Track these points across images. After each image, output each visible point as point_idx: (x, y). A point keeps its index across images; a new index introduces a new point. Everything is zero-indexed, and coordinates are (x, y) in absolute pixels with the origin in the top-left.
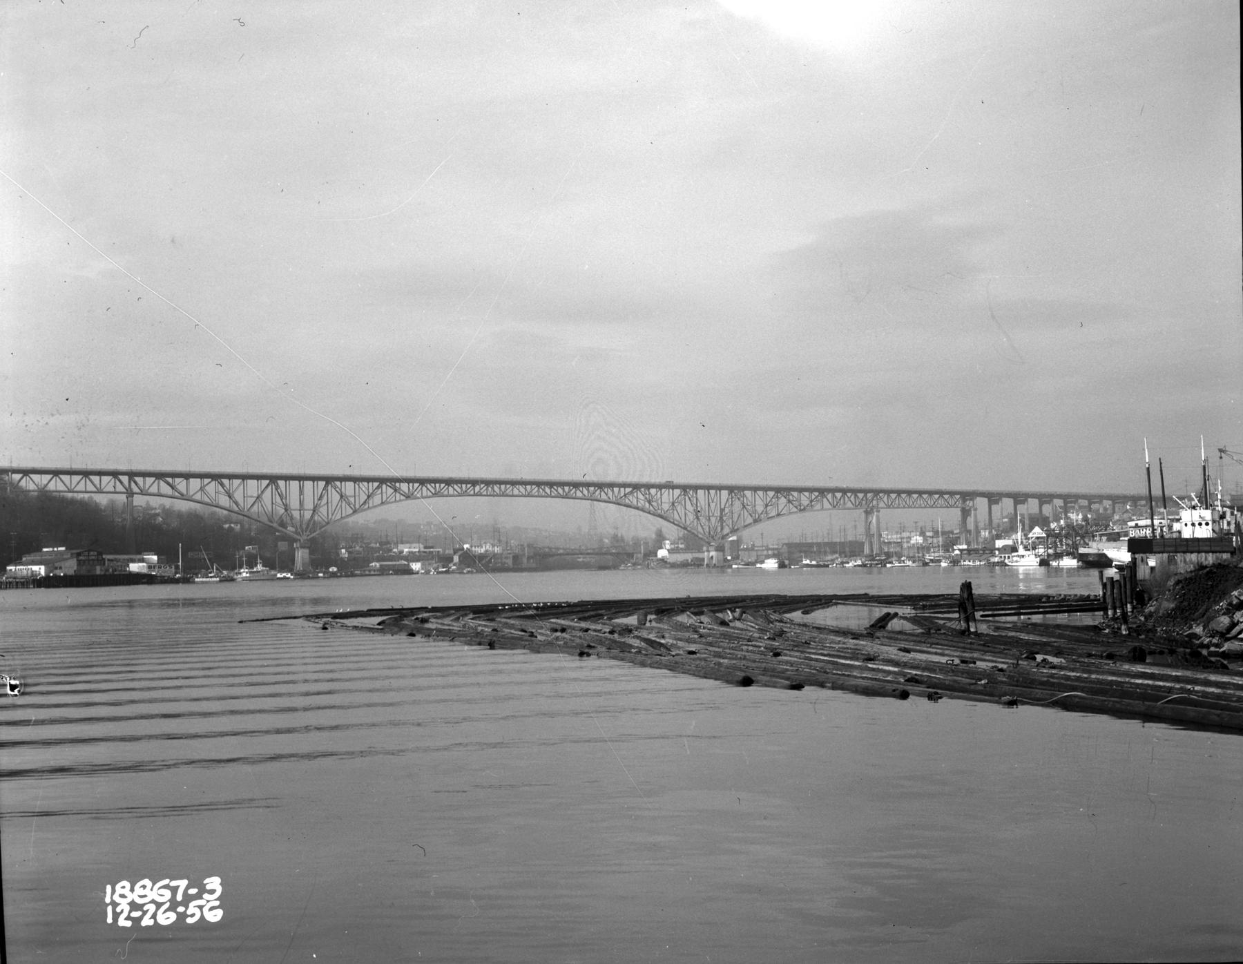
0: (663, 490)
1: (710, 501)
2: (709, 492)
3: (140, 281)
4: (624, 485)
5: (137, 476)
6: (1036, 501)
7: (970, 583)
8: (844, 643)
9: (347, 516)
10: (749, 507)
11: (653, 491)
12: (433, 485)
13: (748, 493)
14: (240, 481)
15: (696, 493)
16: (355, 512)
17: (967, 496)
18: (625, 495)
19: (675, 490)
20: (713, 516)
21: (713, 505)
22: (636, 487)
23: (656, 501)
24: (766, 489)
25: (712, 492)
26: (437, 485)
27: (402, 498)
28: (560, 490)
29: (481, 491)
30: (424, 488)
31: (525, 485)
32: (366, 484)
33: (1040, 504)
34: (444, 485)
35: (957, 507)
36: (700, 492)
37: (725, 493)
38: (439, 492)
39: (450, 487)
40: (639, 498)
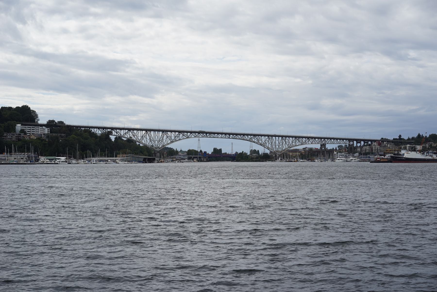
0: (139, 131)
1: (156, 135)
9: (168, 144)
10: (169, 137)
11: (135, 131)
13: (169, 133)
15: (151, 133)
16: (172, 142)
20: (156, 141)
21: (156, 137)
22: (255, 135)
23: (136, 136)
24: (175, 131)
25: (156, 132)
28: (239, 136)
30: (226, 136)
36: (152, 132)
37: (161, 133)
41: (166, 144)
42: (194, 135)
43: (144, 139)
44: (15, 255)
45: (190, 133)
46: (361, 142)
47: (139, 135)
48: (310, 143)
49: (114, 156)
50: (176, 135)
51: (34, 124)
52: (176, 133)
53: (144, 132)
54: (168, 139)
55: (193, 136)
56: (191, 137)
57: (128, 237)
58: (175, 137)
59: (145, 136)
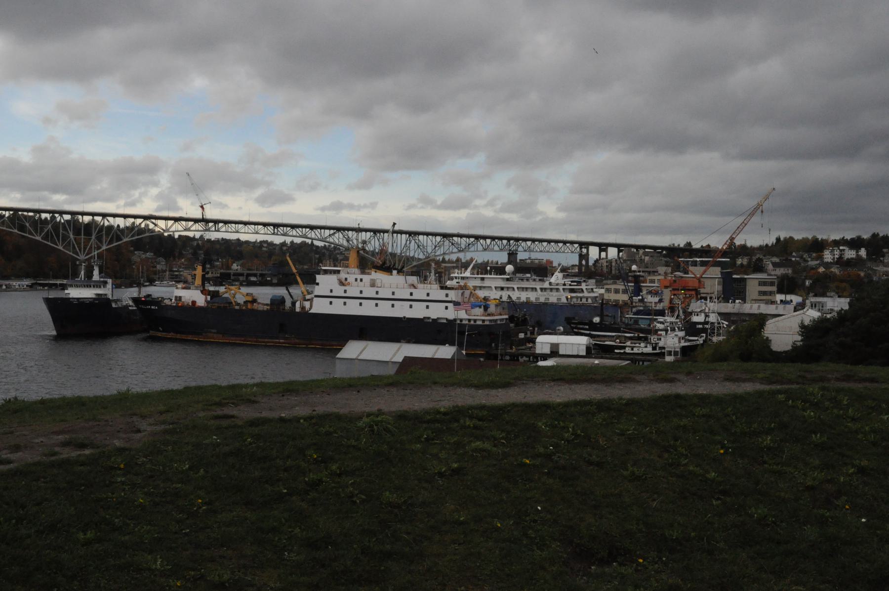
3: (620, 343)
4: (330, 228)
5: (64, 214)
6: (597, 249)
11: (421, 237)
13: (455, 238)
14: (213, 224)
17: (583, 244)
18: (330, 235)
22: (339, 229)
23: (352, 241)
26: (285, 228)
27: (570, 251)
29: (307, 234)
31: (236, 224)
32: (319, 230)
33: (618, 251)
34: (309, 229)
35: (576, 253)
38: (305, 234)
42: (498, 243)
45: (546, 243)
46: (607, 248)
48: (480, 248)
50: (437, 243)
51: (760, 280)
52: (470, 239)
55: (496, 248)
56: (493, 250)
57: (694, 288)
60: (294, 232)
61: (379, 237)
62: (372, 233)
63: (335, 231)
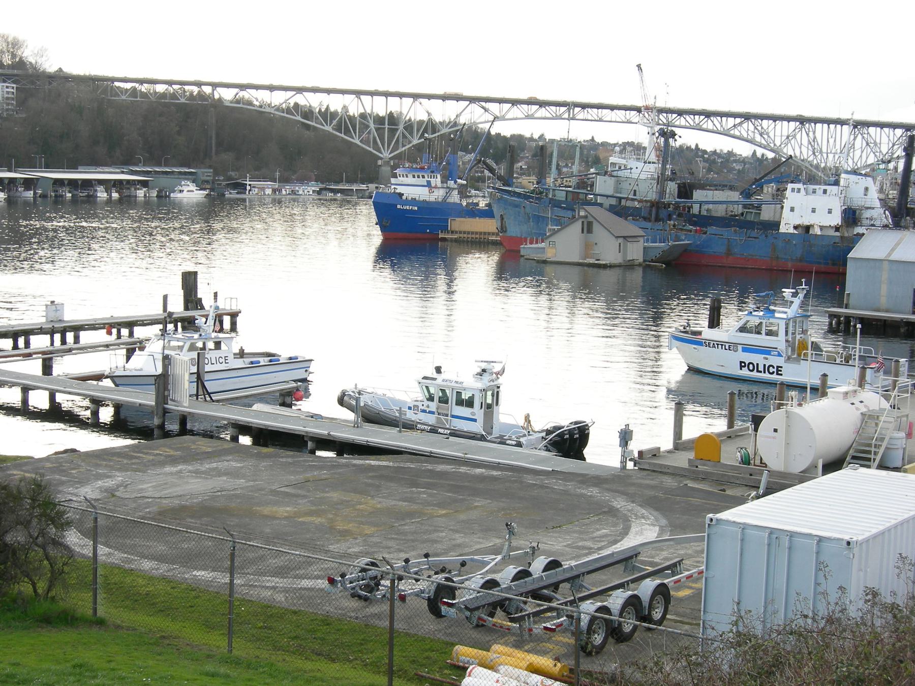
0: (818, 125)
1: (830, 136)
2: (829, 127)
7: (197, 272)
8: (104, 482)
12: (692, 116)
18: (734, 126)
19: (896, 130)
22: (747, 117)
23: (768, 134)
25: (832, 126)
26: (697, 117)
39: (709, 121)
40: (747, 128)
41: (861, 167)
43: (793, 142)
44: (639, 339)
47: (778, 133)
49: (391, 127)
50: (896, 139)
53: (793, 125)
54: (869, 150)
58: (894, 145)
59: (794, 136)
60: (682, 121)
61: (809, 129)
62: (798, 123)
63: (743, 119)
